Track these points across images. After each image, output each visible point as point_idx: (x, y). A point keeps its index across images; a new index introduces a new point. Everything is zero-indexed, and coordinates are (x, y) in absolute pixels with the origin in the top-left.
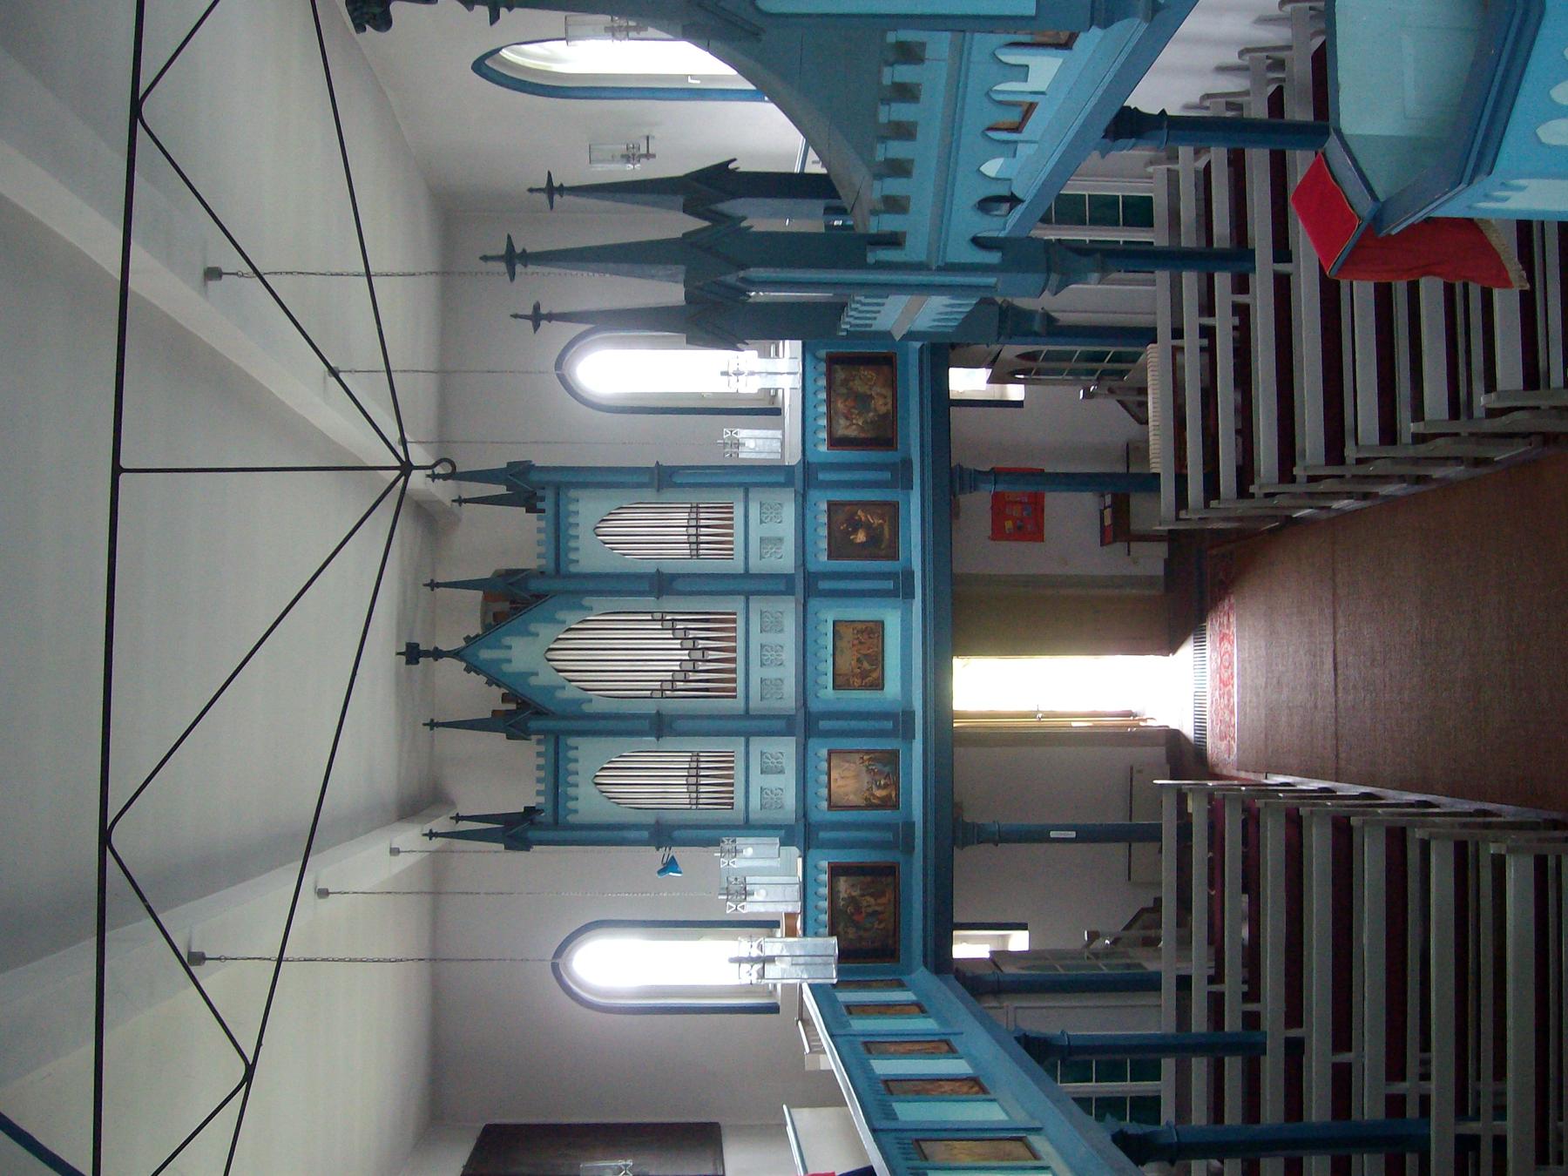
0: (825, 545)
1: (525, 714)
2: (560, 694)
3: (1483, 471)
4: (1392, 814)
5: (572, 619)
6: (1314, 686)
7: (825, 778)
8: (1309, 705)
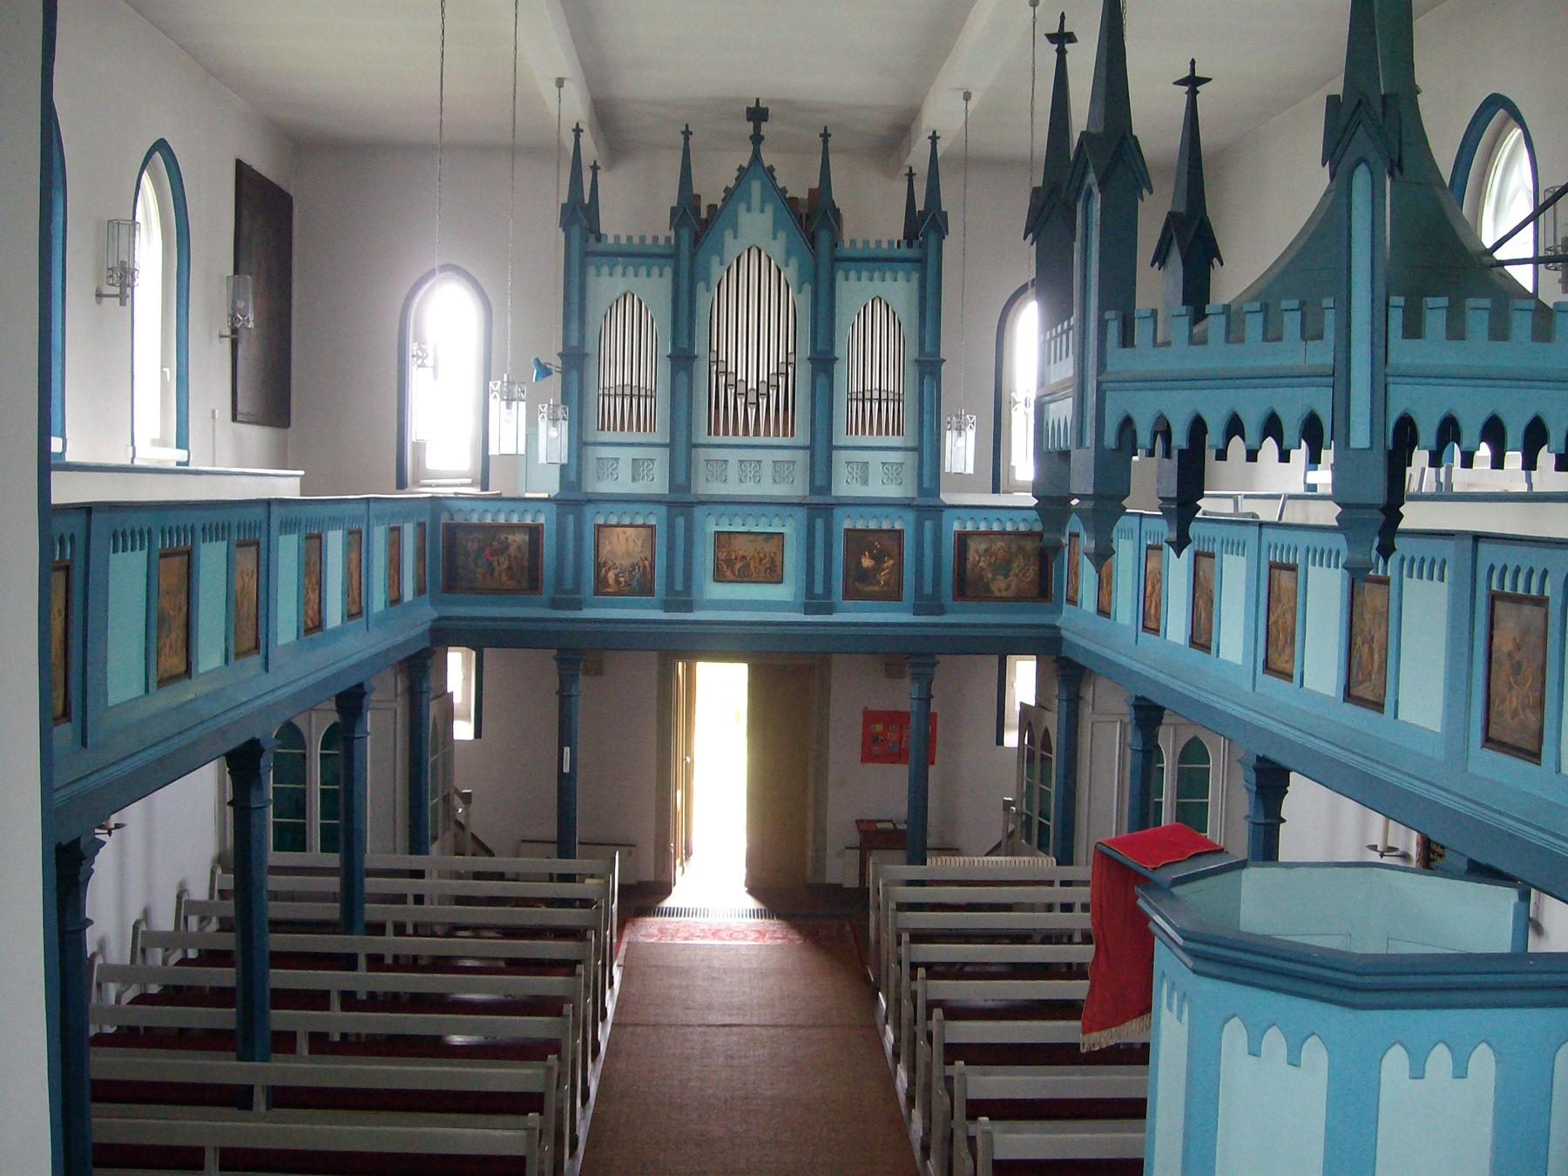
0: (859, 526)
1: (696, 228)
2: (715, 260)
3: (918, 1155)
4: (574, 1053)
5: (789, 274)
6: (709, 1007)
7: (627, 521)
8: (690, 1003)
